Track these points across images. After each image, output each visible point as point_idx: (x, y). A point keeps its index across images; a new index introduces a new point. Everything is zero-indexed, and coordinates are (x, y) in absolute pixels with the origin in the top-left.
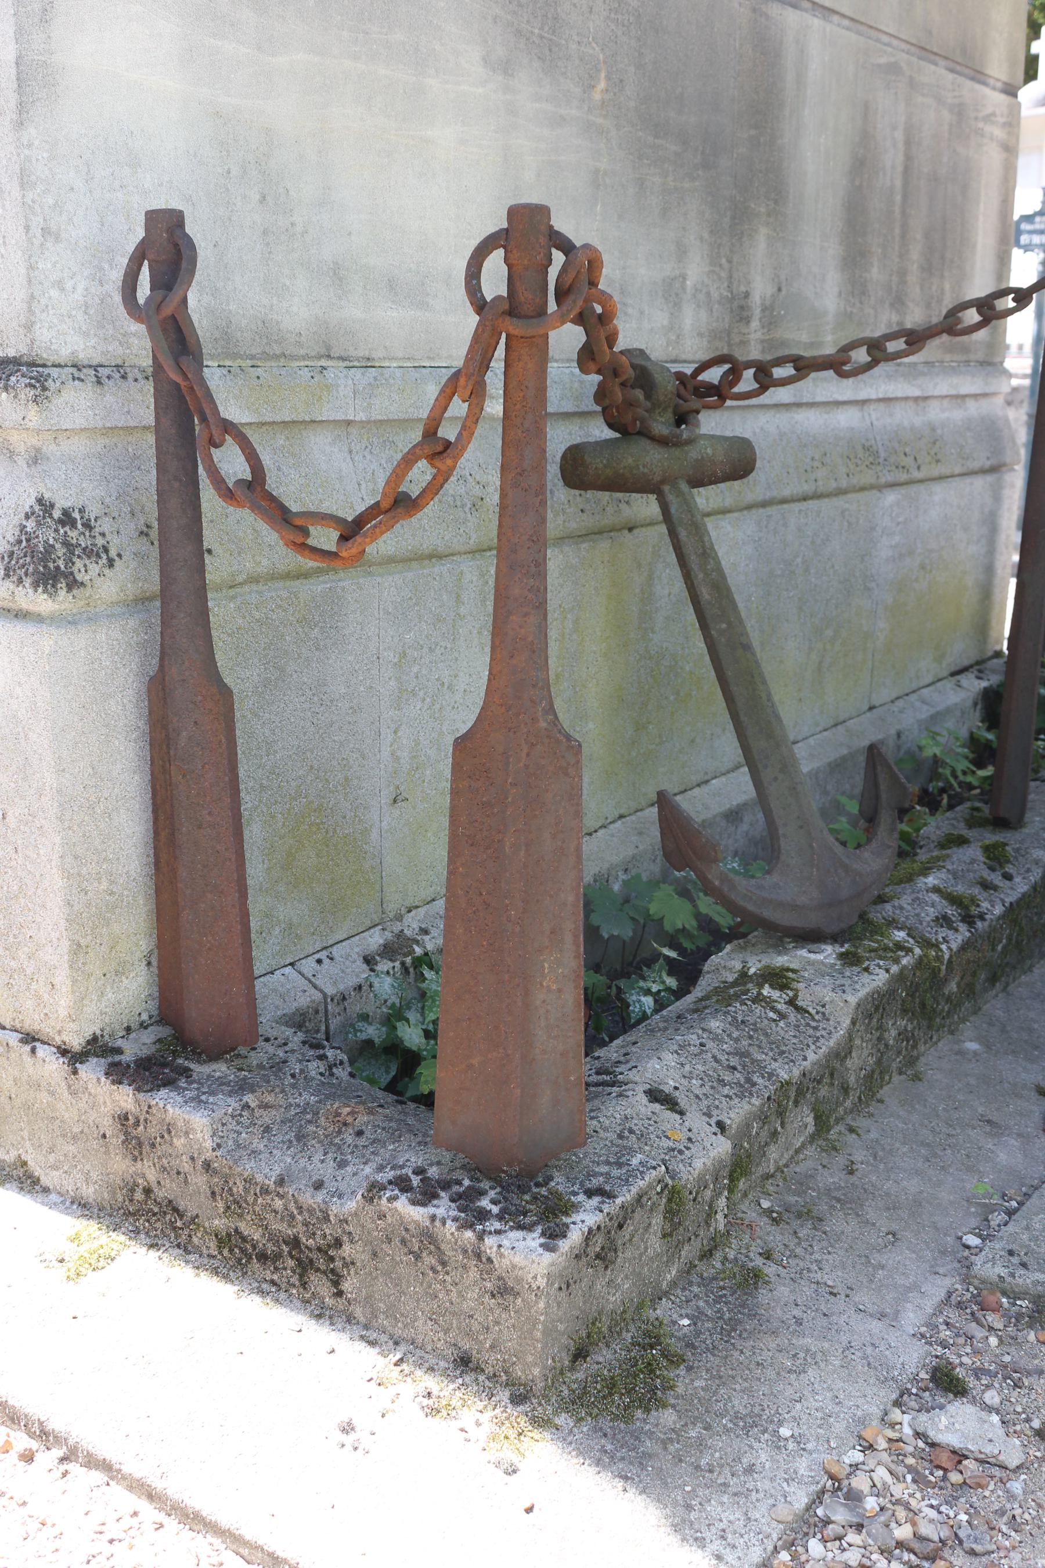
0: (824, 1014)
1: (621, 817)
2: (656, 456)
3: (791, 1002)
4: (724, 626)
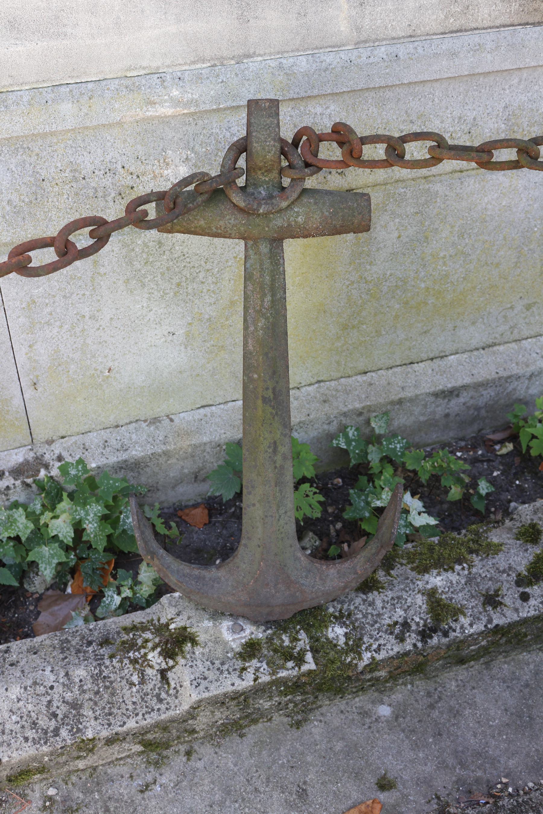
0: (177, 691)
1: (319, 382)
2: (232, 221)
3: (163, 673)
4: (255, 376)
